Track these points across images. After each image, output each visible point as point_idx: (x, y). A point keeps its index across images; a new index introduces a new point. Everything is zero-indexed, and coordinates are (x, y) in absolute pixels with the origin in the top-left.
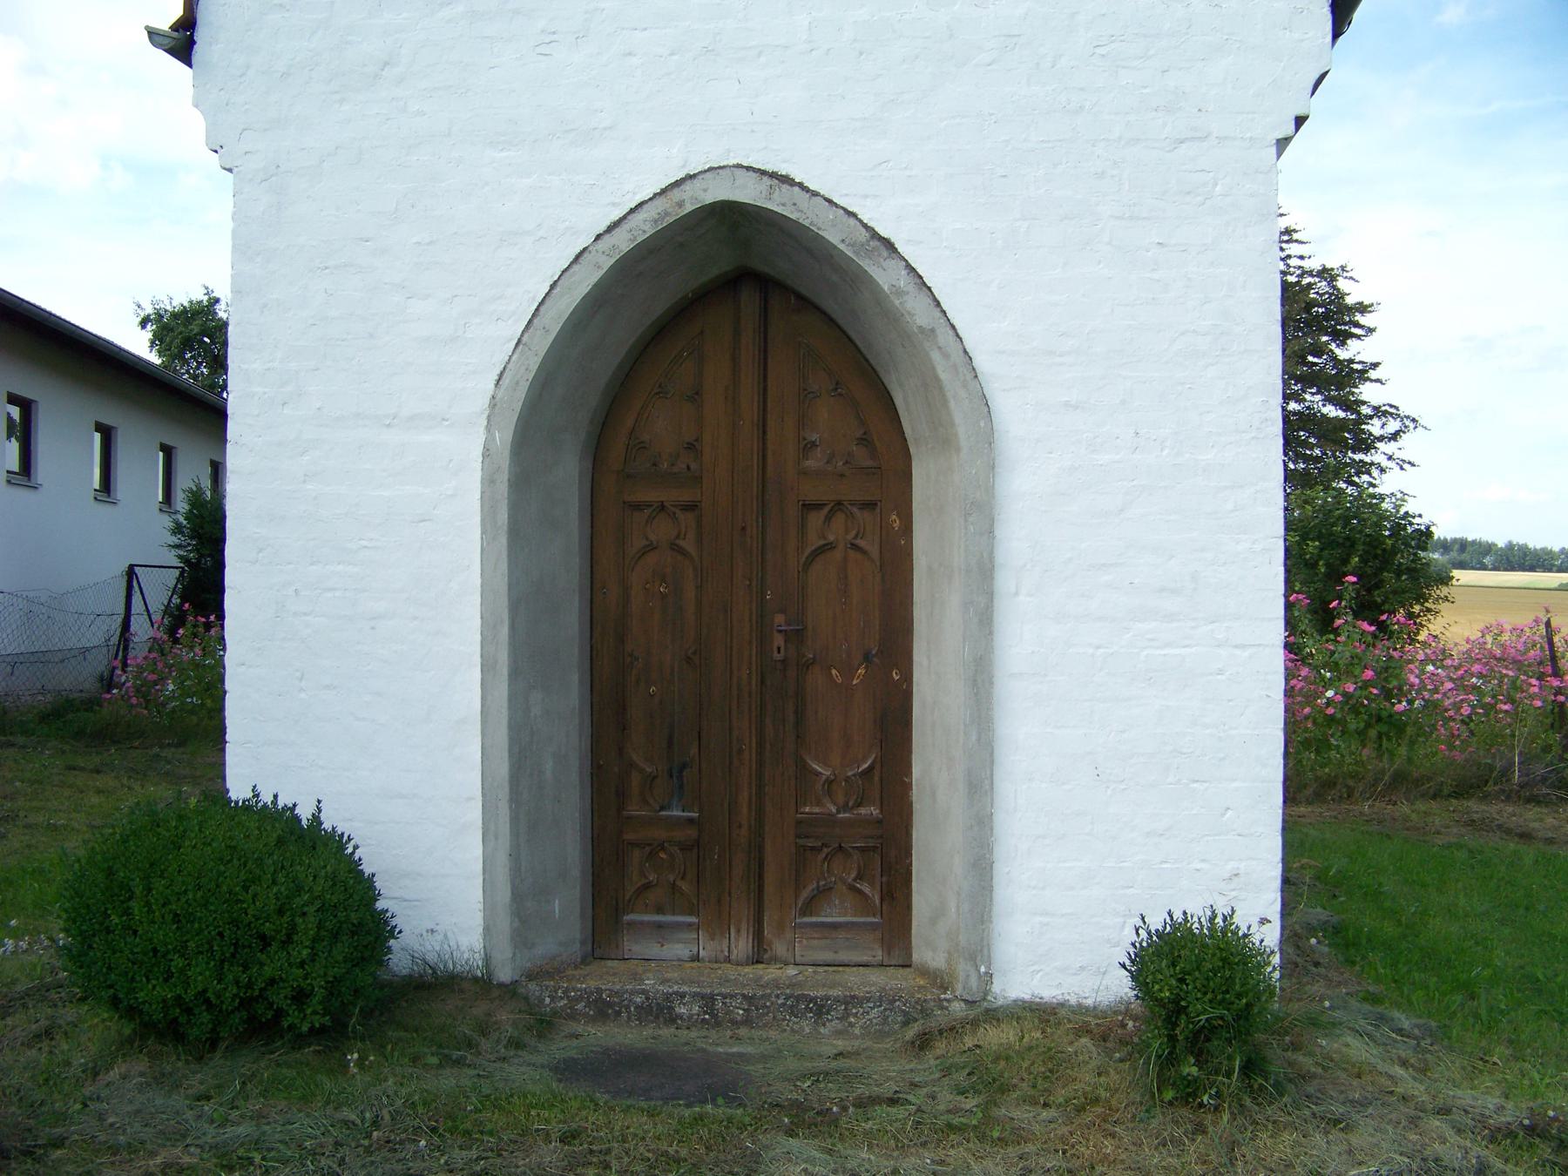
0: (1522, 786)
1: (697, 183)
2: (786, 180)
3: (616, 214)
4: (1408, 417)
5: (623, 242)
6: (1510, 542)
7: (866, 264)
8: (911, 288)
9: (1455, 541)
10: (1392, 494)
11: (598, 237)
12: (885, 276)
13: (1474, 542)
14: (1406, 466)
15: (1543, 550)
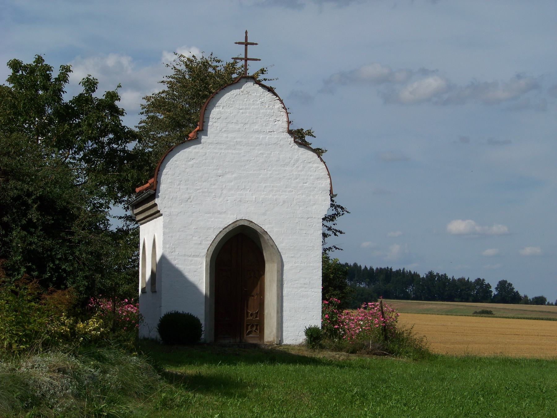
0: (372, 350)
1: (239, 222)
2: (252, 222)
3: (226, 226)
4: (339, 206)
5: (227, 230)
6: (431, 273)
7: (263, 235)
8: (270, 239)
9: (381, 271)
10: (329, 248)
11: (223, 229)
12: (266, 237)
13: (398, 272)
14: (338, 233)
15: (461, 280)
